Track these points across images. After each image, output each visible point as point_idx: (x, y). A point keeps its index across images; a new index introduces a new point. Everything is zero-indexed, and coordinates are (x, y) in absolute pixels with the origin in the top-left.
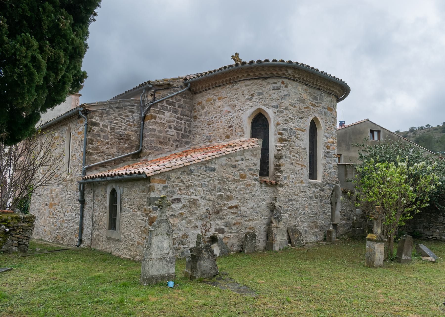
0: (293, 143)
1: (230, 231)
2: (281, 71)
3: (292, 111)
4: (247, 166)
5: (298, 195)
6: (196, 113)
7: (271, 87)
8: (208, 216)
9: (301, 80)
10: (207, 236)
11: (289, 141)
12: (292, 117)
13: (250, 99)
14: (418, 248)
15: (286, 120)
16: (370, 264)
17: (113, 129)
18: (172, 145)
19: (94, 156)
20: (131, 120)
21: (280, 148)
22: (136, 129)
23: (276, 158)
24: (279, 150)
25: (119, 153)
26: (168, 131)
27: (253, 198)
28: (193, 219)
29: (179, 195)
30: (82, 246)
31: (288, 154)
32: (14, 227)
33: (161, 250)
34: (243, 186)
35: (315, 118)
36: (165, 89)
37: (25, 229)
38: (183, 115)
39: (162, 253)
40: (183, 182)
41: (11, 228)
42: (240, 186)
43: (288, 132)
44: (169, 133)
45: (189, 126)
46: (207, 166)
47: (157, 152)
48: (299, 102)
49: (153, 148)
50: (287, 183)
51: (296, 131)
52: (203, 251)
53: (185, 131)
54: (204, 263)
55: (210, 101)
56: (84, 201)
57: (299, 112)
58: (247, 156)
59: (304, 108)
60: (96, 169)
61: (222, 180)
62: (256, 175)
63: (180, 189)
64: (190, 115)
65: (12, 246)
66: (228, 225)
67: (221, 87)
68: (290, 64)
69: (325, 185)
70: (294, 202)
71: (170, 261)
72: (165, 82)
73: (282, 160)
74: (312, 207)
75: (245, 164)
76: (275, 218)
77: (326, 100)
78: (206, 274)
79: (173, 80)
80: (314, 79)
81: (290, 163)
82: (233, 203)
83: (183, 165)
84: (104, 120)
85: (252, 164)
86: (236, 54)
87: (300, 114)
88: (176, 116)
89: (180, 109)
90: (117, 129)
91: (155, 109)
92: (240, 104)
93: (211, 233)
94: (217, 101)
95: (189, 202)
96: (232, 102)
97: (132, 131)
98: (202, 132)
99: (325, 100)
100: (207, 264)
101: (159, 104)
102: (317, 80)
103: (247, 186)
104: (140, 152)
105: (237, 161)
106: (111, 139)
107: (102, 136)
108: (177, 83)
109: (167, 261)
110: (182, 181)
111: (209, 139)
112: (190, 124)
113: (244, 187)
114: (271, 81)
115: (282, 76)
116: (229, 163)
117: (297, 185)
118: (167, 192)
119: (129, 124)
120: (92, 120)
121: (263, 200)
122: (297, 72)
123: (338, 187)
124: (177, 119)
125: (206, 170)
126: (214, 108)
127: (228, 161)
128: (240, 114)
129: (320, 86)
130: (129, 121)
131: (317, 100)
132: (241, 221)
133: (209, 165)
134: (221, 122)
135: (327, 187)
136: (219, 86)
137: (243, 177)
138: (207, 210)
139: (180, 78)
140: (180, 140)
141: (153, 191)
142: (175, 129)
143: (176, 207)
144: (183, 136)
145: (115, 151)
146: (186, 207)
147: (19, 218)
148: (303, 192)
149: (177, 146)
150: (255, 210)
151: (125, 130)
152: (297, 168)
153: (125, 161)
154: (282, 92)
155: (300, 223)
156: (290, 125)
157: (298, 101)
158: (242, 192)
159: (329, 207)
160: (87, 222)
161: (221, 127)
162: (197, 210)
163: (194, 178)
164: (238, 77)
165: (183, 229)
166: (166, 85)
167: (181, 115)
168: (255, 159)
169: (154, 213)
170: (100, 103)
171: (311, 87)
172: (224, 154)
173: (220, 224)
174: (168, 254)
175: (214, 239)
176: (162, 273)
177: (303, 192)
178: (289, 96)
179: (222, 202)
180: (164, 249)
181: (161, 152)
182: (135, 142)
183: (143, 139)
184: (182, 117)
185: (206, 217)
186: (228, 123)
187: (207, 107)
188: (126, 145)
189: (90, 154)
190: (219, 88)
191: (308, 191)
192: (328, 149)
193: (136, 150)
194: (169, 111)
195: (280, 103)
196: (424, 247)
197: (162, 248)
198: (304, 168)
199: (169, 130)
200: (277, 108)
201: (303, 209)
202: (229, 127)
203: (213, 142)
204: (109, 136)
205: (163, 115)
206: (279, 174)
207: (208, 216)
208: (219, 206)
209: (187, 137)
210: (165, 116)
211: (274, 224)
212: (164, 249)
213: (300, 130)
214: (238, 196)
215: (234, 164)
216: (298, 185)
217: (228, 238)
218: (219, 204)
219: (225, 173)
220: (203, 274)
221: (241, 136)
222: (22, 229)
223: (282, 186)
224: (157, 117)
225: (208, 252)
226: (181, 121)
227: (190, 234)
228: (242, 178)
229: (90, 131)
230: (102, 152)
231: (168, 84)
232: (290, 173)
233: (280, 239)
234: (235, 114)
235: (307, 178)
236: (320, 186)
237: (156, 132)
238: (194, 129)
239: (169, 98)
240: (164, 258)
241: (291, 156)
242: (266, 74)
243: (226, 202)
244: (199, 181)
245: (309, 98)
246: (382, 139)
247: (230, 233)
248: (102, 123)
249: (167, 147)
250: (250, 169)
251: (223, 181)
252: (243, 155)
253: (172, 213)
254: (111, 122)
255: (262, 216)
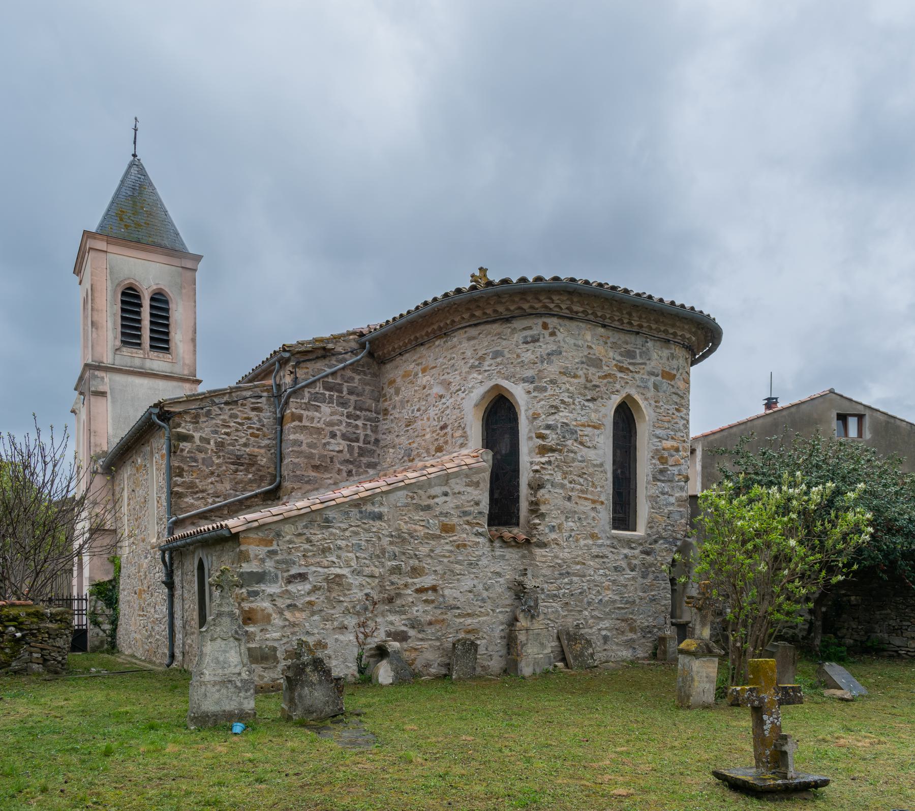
0: (572, 455)
1: (420, 636)
2: (540, 301)
3: (568, 386)
4: (457, 507)
5: (584, 564)
6: (387, 403)
7: (518, 337)
8: (370, 608)
9: (591, 317)
10: (369, 646)
11: (560, 451)
12: (566, 400)
13: (477, 367)
14: (821, 672)
15: (552, 406)
16: (683, 702)
17: (220, 445)
18: (339, 471)
19: (186, 500)
20: (257, 426)
21: (537, 467)
22: (267, 442)
23: (532, 488)
24: (536, 471)
25: (236, 491)
26: (328, 443)
27: (474, 570)
28: (337, 612)
29: (303, 567)
30: (174, 665)
31: (558, 477)
32: (31, 630)
33: (223, 668)
34: (448, 547)
35: (629, 396)
36: (317, 358)
37: (54, 633)
38: (361, 409)
39: (227, 671)
40: (311, 542)
41: (25, 632)
42: (444, 547)
43: (559, 431)
44: (331, 448)
45: (375, 430)
46: (364, 509)
47: (308, 487)
48: (585, 366)
49: (299, 479)
50: (556, 539)
51: (578, 429)
52: (308, 670)
53: (366, 442)
54: (311, 692)
55: (409, 375)
56: (173, 583)
57: (586, 388)
58: (457, 485)
59: (599, 377)
60: (193, 524)
61: (399, 537)
62: (478, 523)
63: (304, 556)
64: (374, 409)
65: (31, 662)
66: (414, 624)
67: (427, 346)
68: (556, 284)
69: (656, 541)
70: (575, 579)
71: (243, 687)
72: (318, 345)
73: (542, 491)
74: (622, 588)
75: (452, 502)
76: (523, 611)
77: (658, 357)
78: (316, 711)
79: (335, 339)
80: (620, 310)
81: (564, 498)
82: (427, 581)
83: (308, 510)
84: (201, 428)
85: (468, 502)
86: (481, 269)
87: (587, 392)
88: (346, 411)
89: (353, 398)
90: (229, 445)
91: (298, 401)
92: (458, 378)
93: (376, 640)
94: (420, 375)
95: (326, 579)
96: (446, 376)
97: (259, 447)
98: (397, 441)
99: (655, 356)
100: (316, 694)
101: (306, 390)
102: (630, 314)
103: (458, 547)
104: (279, 487)
105: (434, 497)
106: (219, 466)
107: (200, 461)
108: (344, 344)
109: (236, 687)
110: (309, 541)
111: (409, 455)
112: (377, 426)
113: (451, 548)
114: (518, 324)
115: (543, 311)
116: (414, 502)
117: (582, 542)
118: (277, 562)
119: (252, 435)
120: (179, 430)
121: (498, 574)
122: (575, 300)
123: (691, 544)
124: (348, 417)
125: (361, 518)
126: (415, 391)
127: (413, 498)
128: (459, 399)
129: (641, 326)
130: (253, 428)
131: (634, 357)
132: (445, 617)
133: (369, 508)
134: (428, 419)
135: (660, 545)
136: (422, 344)
137: (447, 529)
138: (367, 595)
139: (350, 333)
140: (355, 460)
141: (247, 559)
142: (344, 437)
143: (299, 591)
144: (362, 452)
145: (228, 488)
146: (319, 589)
147: (43, 615)
148: (597, 556)
149: (350, 473)
150: (479, 595)
151: (245, 445)
152: (582, 508)
153: (249, 507)
154: (544, 346)
155: (591, 621)
156: (564, 416)
157: (583, 363)
158: (446, 560)
159: (664, 588)
160: (178, 623)
161: (428, 430)
162: (345, 595)
163: (334, 535)
164: (453, 322)
165: (316, 631)
166: (320, 351)
167: (355, 408)
168: (477, 492)
169: (252, 602)
170: (190, 396)
171: (616, 329)
172: (402, 484)
173: (397, 623)
174: (239, 674)
175: (381, 652)
176: (227, 708)
177: (597, 556)
178: (560, 353)
179: (400, 581)
180: (230, 666)
181: (316, 486)
182: (268, 468)
183: (281, 461)
184: (358, 413)
185: (366, 609)
186: (439, 421)
187: (403, 389)
188: (250, 476)
189: (180, 495)
190: (422, 348)
191: (610, 555)
192: (662, 463)
193: (270, 484)
194: (329, 403)
195: (540, 371)
196: (835, 670)
197: (225, 663)
198: (599, 507)
199: (331, 440)
200: (532, 382)
201: (598, 592)
202: (442, 428)
203: (416, 461)
204: (214, 459)
205: (317, 411)
206: (537, 521)
207: (370, 608)
208: (392, 587)
209: (372, 453)
210: (320, 413)
211: (523, 622)
212: (230, 666)
213: (589, 426)
214: (437, 568)
215: (426, 503)
216: (586, 542)
217: (416, 649)
218: (392, 583)
219: (406, 523)
220: (309, 711)
221: (462, 446)
222: (47, 632)
223: (543, 545)
224: (305, 416)
225: (318, 672)
226: (357, 422)
227: (330, 641)
228: (447, 532)
229: (175, 452)
230: (203, 491)
231: (324, 349)
232: (563, 518)
233: (536, 653)
234: (451, 401)
235: (608, 527)
236: (641, 544)
237: (304, 447)
238: (384, 437)
239: (327, 376)
240: (230, 681)
241: (566, 482)
242: (508, 310)
243: (410, 581)
244: (347, 539)
245: (611, 354)
246: (868, 435)
247: (422, 640)
248: (199, 434)
249: (329, 476)
250: (465, 513)
251: (400, 538)
252: (446, 484)
253: (289, 602)
254: (216, 432)
255: (497, 607)
